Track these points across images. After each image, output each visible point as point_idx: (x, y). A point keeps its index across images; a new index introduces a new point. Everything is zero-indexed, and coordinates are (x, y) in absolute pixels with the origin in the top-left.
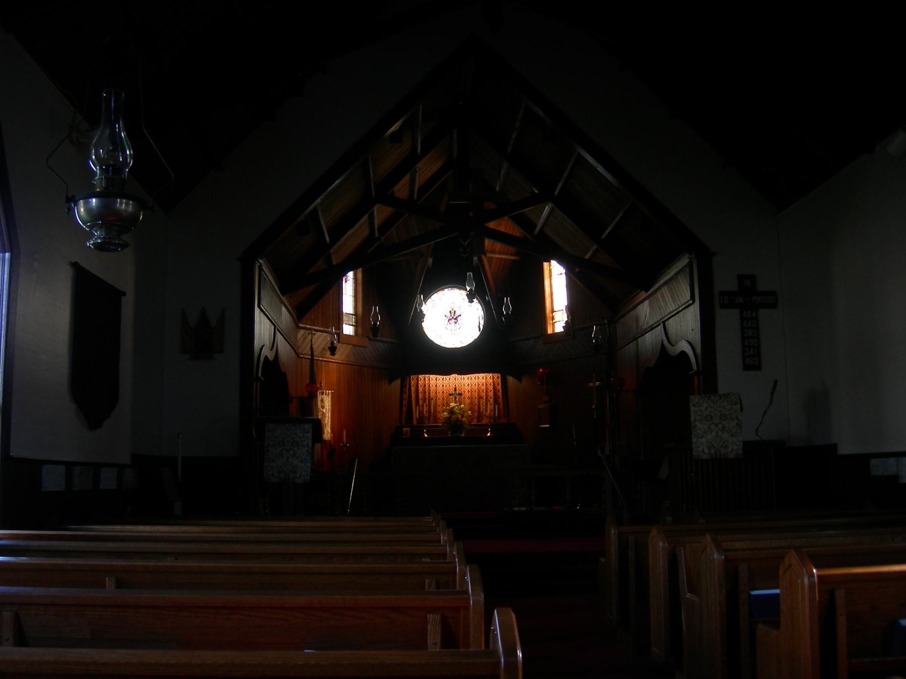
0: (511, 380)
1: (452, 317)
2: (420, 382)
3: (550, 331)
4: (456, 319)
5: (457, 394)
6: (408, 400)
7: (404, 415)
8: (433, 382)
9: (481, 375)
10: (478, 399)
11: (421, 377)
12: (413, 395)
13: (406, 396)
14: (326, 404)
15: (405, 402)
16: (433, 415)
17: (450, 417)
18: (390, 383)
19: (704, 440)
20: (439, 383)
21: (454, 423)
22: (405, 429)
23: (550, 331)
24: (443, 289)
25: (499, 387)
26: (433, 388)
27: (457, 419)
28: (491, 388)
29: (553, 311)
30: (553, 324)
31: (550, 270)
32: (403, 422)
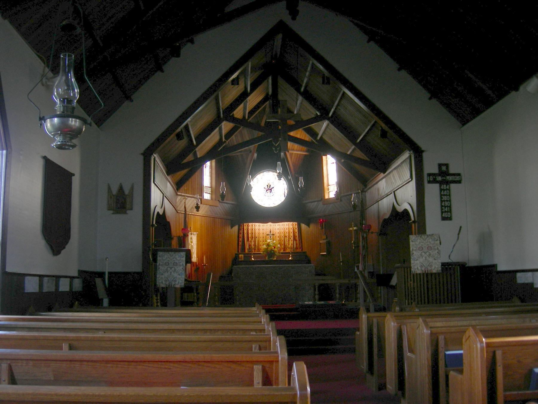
0: (303, 226)
3: (326, 197)
4: (271, 190)
5: (271, 235)
6: (242, 239)
7: (240, 247)
8: (257, 228)
12: (246, 235)
13: (241, 236)
15: (241, 239)
17: (267, 248)
19: (418, 262)
20: (260, 229)
22: (240, 255)
23: (326, 197)
25: (297, 230)
26: (257, 231)
27: (272, 250)
28: (292, 231)
29: (328, 185)
30: (329, 193)
31: (327, 161)
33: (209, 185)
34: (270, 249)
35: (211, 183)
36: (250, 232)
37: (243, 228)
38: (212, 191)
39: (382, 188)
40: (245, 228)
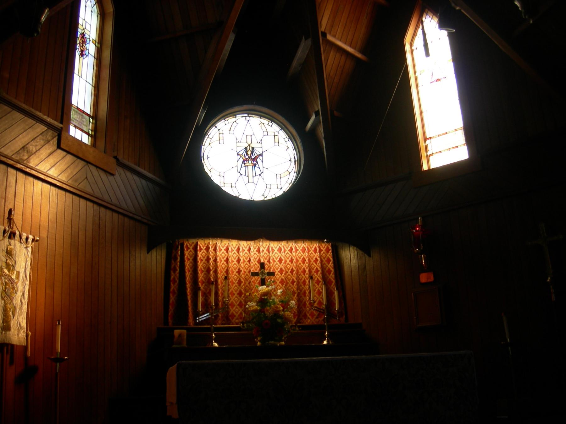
0: (350, 256)
1: (249, 156)
2: (199, 253)
3: (425, 168)
4: (255, 159)
5: (264, 273)
6: (183, 288)
7: (171, 309)
8: (221, 254)
9: (300, 245)
10: (297, 287)
11: (202, 243)
12: (188, 275)
13: (174, 276)
14: (273, 342)
15: (173, 287)
16: (222, 311)
17: (262, 311)
18: (149, 251)
20: (233, 254)
21: (267, 321)
22: (177, 332)
23: (425, 168)
24: (234, 114)
25: (330, 266)
26: (221, 265)
27: (276, 314)
28: (318, 266)
29: (425, 139)
30: (428, 157)
31: (416, 78)
32: (170, 321)
33: (88, 109)
34: (269, 311)
35: (96, 104)
36: (200, 265)
37: (182, 255)
38: (95, 129)
39: (348, 260)
40: (187, 254)
